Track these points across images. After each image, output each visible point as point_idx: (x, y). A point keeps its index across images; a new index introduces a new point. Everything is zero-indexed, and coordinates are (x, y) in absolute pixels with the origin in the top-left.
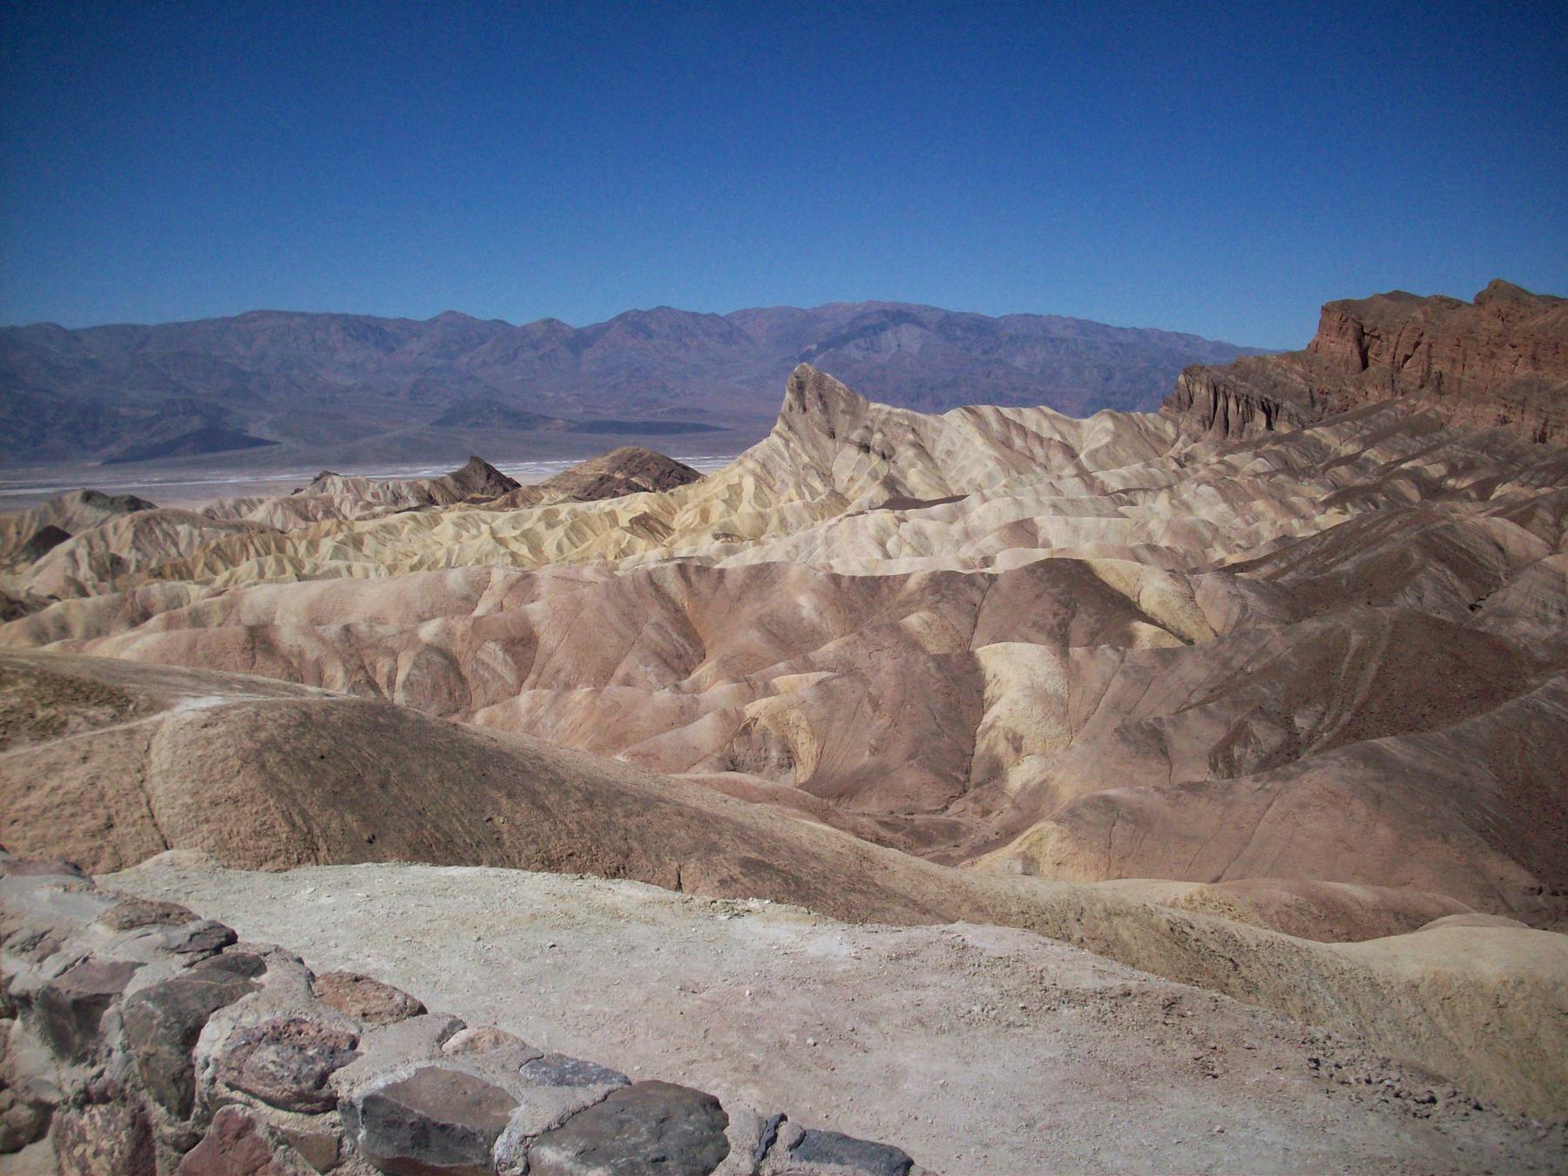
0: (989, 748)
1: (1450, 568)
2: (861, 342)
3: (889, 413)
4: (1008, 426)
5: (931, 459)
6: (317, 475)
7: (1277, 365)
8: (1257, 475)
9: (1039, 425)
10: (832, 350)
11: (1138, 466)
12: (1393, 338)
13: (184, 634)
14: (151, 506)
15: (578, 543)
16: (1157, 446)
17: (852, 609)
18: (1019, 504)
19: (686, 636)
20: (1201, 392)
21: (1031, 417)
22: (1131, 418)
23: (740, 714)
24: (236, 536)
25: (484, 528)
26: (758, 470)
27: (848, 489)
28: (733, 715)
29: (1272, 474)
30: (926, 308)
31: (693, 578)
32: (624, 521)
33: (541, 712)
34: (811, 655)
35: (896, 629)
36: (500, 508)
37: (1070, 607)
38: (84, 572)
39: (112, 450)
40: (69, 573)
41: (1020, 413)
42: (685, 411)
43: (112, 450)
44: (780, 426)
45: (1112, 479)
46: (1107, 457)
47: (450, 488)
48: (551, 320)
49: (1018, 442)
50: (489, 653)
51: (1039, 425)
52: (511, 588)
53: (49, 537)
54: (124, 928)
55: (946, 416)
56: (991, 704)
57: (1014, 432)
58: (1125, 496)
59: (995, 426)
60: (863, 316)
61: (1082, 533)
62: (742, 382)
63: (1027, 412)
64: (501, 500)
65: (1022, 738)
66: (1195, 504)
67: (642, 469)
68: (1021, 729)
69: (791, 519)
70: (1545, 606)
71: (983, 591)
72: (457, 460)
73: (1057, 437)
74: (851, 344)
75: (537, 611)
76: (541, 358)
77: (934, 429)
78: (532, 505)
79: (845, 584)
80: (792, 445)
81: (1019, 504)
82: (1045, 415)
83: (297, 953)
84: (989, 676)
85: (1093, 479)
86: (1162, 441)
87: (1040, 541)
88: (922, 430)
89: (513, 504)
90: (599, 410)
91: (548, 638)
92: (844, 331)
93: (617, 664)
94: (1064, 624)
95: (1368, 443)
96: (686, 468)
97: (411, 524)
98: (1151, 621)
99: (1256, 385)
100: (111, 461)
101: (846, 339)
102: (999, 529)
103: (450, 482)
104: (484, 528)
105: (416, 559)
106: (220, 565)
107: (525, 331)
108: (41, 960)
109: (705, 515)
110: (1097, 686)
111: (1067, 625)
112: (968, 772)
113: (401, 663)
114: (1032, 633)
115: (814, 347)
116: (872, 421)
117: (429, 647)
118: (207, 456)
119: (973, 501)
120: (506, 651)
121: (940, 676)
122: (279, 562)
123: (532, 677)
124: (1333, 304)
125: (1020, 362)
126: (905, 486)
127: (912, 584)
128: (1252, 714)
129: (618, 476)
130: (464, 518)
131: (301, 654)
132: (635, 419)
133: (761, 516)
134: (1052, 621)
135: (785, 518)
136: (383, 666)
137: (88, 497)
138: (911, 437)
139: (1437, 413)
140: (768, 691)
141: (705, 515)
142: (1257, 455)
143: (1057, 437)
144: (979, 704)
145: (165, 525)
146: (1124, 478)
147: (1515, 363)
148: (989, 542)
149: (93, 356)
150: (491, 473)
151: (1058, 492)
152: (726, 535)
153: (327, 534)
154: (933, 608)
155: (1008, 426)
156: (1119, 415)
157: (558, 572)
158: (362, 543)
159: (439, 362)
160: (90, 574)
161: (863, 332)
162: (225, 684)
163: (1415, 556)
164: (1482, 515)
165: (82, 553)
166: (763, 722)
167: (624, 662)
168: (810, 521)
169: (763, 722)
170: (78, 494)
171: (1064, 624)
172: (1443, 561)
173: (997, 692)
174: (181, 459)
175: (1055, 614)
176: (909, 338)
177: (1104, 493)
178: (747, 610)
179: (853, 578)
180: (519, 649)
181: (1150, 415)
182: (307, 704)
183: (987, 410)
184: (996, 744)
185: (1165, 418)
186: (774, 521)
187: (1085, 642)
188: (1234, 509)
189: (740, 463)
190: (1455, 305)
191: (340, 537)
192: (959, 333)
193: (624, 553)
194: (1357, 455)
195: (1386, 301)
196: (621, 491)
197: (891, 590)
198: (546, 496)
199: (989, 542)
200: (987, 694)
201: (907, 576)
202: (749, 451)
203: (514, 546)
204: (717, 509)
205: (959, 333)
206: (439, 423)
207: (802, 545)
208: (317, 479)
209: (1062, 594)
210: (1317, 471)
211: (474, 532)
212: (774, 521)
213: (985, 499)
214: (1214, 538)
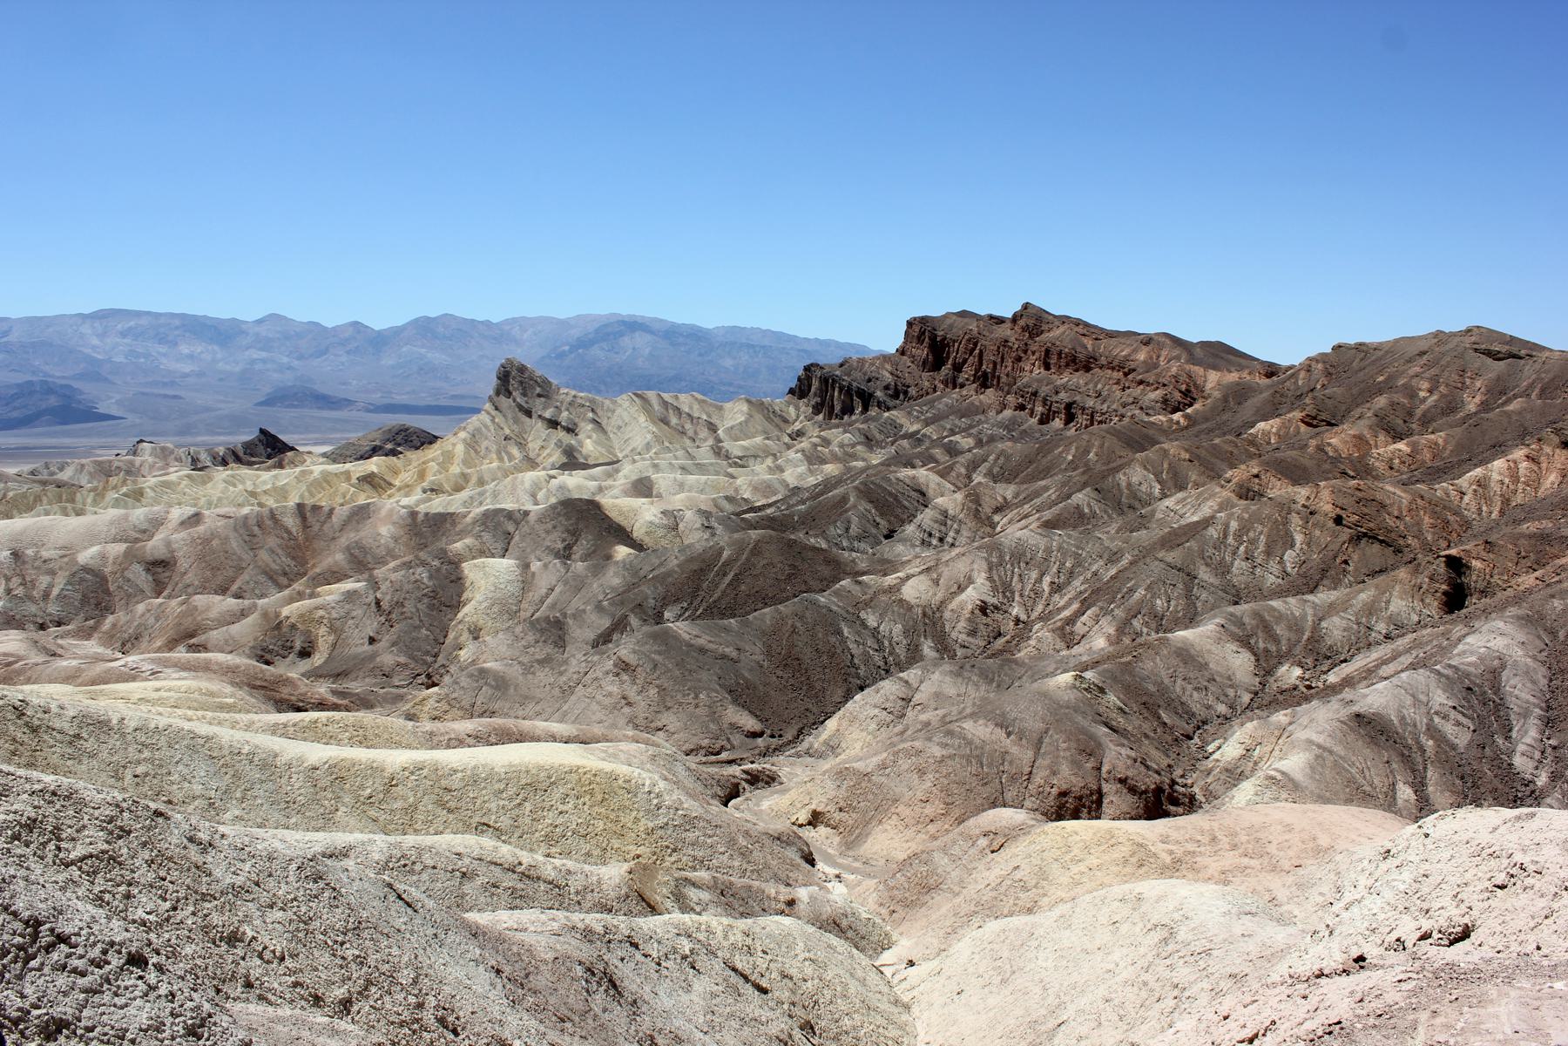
1: (876, 508)
2: (604, 345)
3: (575, 397)
4: (667, 409)
5: (604, 431)
7: (873, 364)
9: (691, 408)
10: (580, 351)
11: (758, 440)
12: (956, 344)
23: (277, 615)
28: (272, 615)
37: (575, 534)
41: (677, 398)
42: (462, 397)
46: (740, 432)
48: (356, 323)
49: (674, 421)
50: (134, 572)
51: (691, 408)
54: (909, 905)
55: (619, 400)
60: (606, 326)
61: (686, 487)
70: (930, 535)
71: (517, 523)
73: (705, 417)
74: (596, 346)
77: (609, 410)
80: (497, 420)
82: (696, 399)
83: (1315, 969)
86: (786, 421)
87: (654, 493)
88: (599, 411)
90: (394, 396)
94: (569, 547)
95: (927, 423)
101: (592, 343)
108: (907, 1007)
111: (571, 548)
112: (436, 656)
113: (57, 581)
116: (562, 402)
117: (86, 569)
118: (59, 428)
124: (915, 319)
125: (728, 363)
127: (468, 519)
128: (632, 610)
130: (233, 476)
132: (422, 403)
134: (560, 546)
136: (44, 581)
138: (590, 415)
139: (980, 402)
141: (422, 475)
143: (705, 417)
144: (456, 606)
147: (1034, 364)
155: (667, 409)
158: (142, 495)
159: (264, 354)
162: (773, 529)
163: (852, 499)
164: (144, 669)
171: (569, 547)
172: (872, 502)
174: (40, 430)
175: (564, 540)
176: (641, 341)
182: (727, 915)
190: (1000, 321)
194: (918, 432)
195: (954, 317)
200: (465, 596)
205: (681, 340)
209: (572, 525)
210: (887, 443)
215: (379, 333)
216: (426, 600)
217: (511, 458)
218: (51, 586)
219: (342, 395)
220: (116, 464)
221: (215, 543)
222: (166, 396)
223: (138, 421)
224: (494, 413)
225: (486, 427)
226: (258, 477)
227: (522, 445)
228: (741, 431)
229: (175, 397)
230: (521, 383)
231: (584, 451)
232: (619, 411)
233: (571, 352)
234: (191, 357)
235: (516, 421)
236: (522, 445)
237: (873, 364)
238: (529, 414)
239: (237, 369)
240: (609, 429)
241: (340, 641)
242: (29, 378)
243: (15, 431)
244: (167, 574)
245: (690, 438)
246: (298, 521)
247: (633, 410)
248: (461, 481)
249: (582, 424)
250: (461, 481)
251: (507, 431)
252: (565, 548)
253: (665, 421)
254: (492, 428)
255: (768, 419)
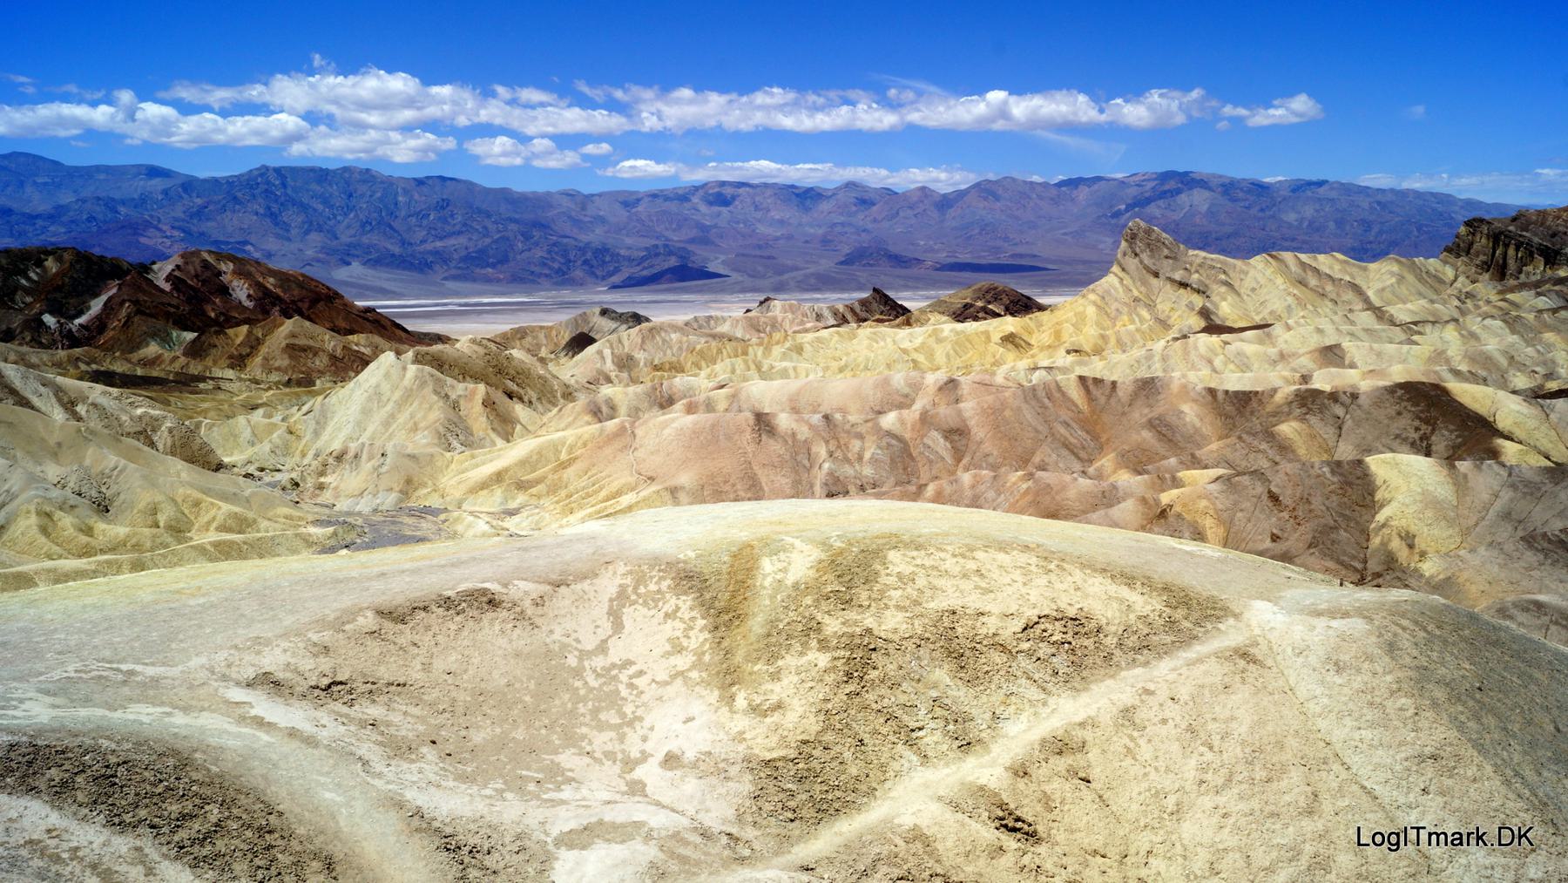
0: (1384, 544)
2: (1161, 203)
5: (1238, 294)
6: (762, 299)
8: (1540, 311)
13: (700, 418)
14: (647, 320)
15: (961, 353)
16: (1437, 285)
17: (1227, 416)
18: (1319, 331)
19: (104, 373)
20: (1482, 242)
21: (1324, 262)
22: (1414, 263)
23: (1157, 502)
24: (714, 344)
25: (889, 340)
26: (1099, 302)
27: (1169, 317)
29: (1555, 311)
30: (1214, 176)
31: (1091, 387)
32: (996, 337)
33: (982, 488)
34: (1198, 453)
35: (1270, 436)
36: (898, 326)
38: (609, 365)
39: (616, 279)
40: (598, 365)
41: (1316, 259)
42: (1021, 256)
43: (616, 279)
44: (1115, 268)
45: (1401, 312)
47: (858, 310)
52: (940, 389)
53: (581, 341)
55: (1252, 261)
56: (1382, 506)
57: (1310, 273)
58: (1412, 329)
59: (1294, 267)
62: (1065, 234)
63: (1321, 257)
64: (901, 319)
65: (1414, 536)
66: (1483, 335)
67: (996, 299)
68: (1413, 529)
69: (1126, 339)
72: (860, 288)
75: (968, 407)
76: (915, 216)
77: (1242, 271)
78: (922, 325)
79: (1220, 396)
81: (1319, 331)
82: (1337, 259)
84: (1379, 482)
85: (1383, 313)
86: (1442, 282)
87: (1347, 362)
89: (908, 323)
91: (979, 431)
92: (1147, 195)
93: (1033, 453)
96: (1029, 298)
97: (836, 338)
98: (1509, 438)
99: (1536, 234)
100: (614, 287)
102: (1315, 350)
103: (858, 308)
104: (889, 340)
105: (843, 363)
106: (703, 364)
107: (905, 196)
109: (1057, 334)
110: (1485, 496)
112: (1365, 562)
113: (867, 445)
114: (1395, 444)
115: (1123, 207)
119: (1277, 330)
120: (946, 438)
121: (1335, 479)
122: (746, 362)
123: (965, 461)
125: (1291, 217)
126: (1216, 315)
127: (1279, 397)
129: (980, 304)
131: (794, 435)
132: (984, 262)
133: (1103, 337)
135: (443, 343)
136: (856, 445)
137: (604, 312)
140: (1176, 483)
141: (1057, 334)
142: (1539, 294)
145: (663, 334)
146: (1412, 312)
148: (1305, 363)
149: (602, 213)
150: (887, 301)
151: (1352, 323)
152: (1076, 351)
153: (778, 343)
154: (1302, 419)
156: (1403, 260)
157: (977, 379)
158: (802, 349)
159: (842, 219)
160: (612, 368)
161: (1163, 195)
165: (607, 352)
166: (1177, 508)
167: (1038, 453)
168: (1142, 342)
169: (1177, 508)
170: (597, 310)
173: (1387, 496)
176: (1199, 200)
177: (1392, 323)
178: (1136, 415)
179: (1227, 392)
180: (956, 438)
181: (1432, 260)
183: (1288, 256)
184: (1390, 540)
185: (1445, 262)
186: (1113, 341)
187: (1446, 455)
188: (1526, 341)
189: (1084, 296)
191: (788, 345)
192: (1241, 195)
193: (997, 363)
196: (980, 315)
197: (1260, 402)
198: (933, 319)
199: (1305, 363)
200: (1379, 496)
201: (1275, 390)
202: (1091, 287)
203: (915, 356)
204: (1068, 329)
205: (1241, 195)
206: (842, 263)
207: (1143, 361)
208: (761, 303)
209: (1422, 412)
211: (882, 344)
212: (1113, 341)
213: (1289, 328)
214: (1510, 364)
215: (944, 196)
216: (1335, 498)
217: (1142, 320)
218: (863, 449)
219: (910, 255)
220: (763, 319)
221: (1007, 413)
222: (761, 257)
223: (741, 279)
224: (1122, 274)
225: (1115, 289)
226: (896, 334)
227: (1151, 307)
228: (1394, 293)
229: (769, 258)
230: (1149, 245)
231: (1220, 313)
232: (1252, 273)
233: (1127, 210)
234: (782, 222)
235: (1144, 283)
236: (1151, 307)
237: (1558, 218)
238: (1156, 275)
239: (820, 231)
240: (1242, 291)
241: (1232, 535)
242: (654, 242)
243: (645, 288)
244: (964, 442)
245: (1332, 300)
246: (1082, 392)
247: (1269, 272)
248: (1100, 342)
249: (1215, 287)
250: (1100, 342)
251: (1136, 293)
252: (1421, 439)
253: (1302, 283)
254: (1121, 290)
255: (1420, 279)
